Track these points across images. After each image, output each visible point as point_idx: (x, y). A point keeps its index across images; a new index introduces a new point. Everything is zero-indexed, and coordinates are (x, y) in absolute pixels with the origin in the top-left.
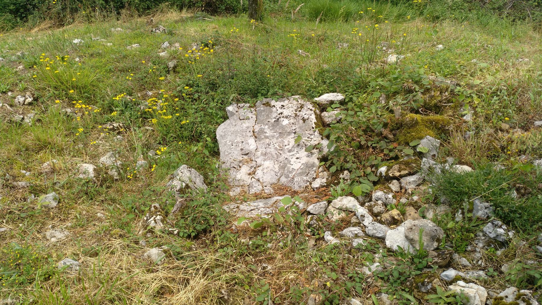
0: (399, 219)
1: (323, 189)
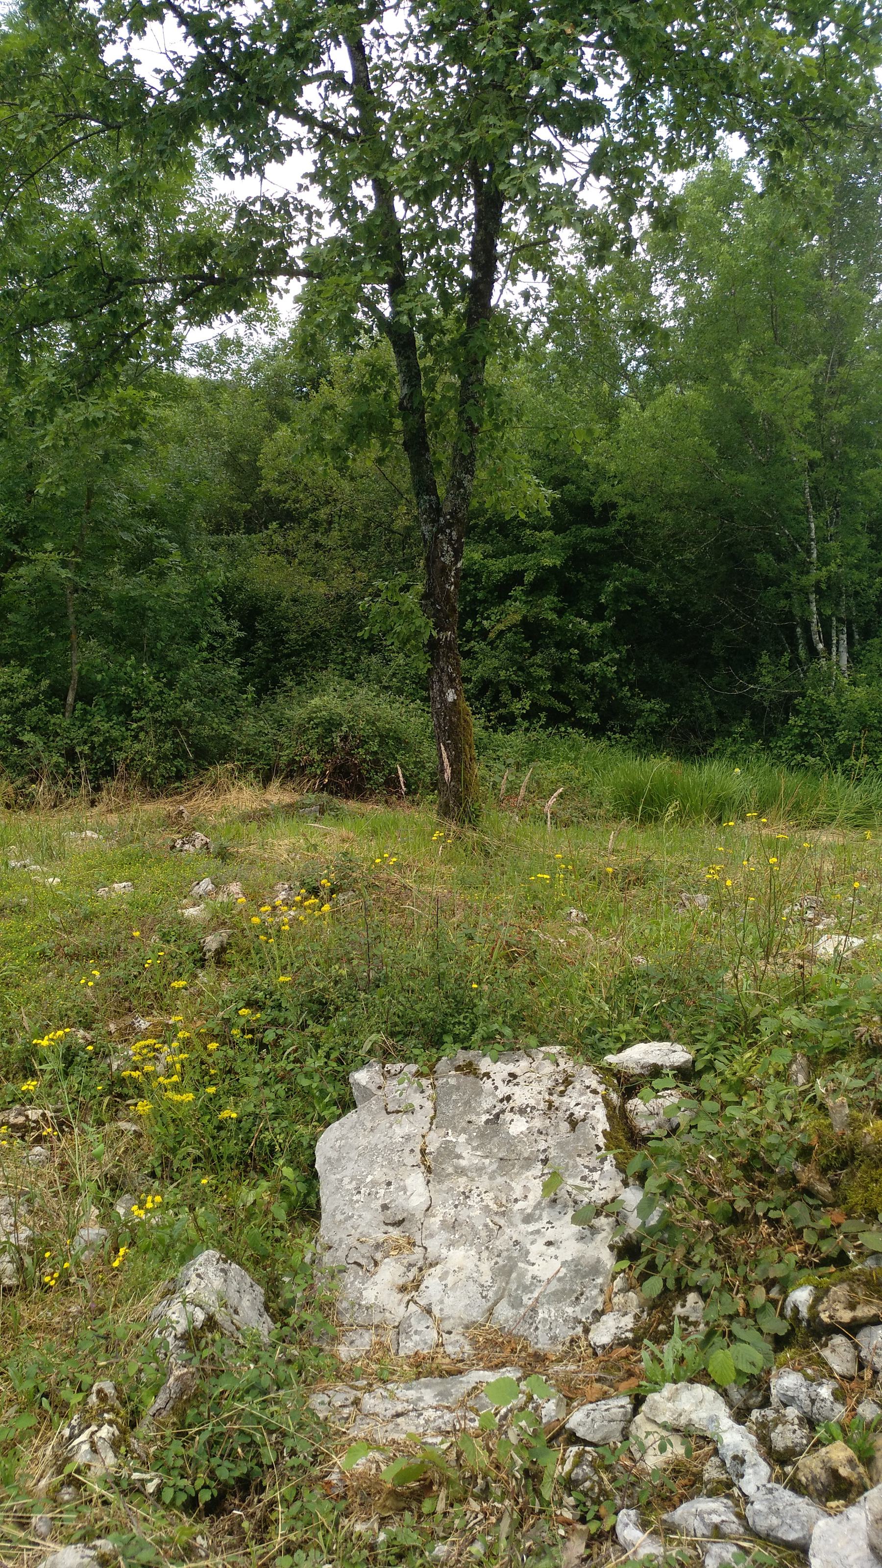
0: (854, 1477)
1: (623, 1351)
